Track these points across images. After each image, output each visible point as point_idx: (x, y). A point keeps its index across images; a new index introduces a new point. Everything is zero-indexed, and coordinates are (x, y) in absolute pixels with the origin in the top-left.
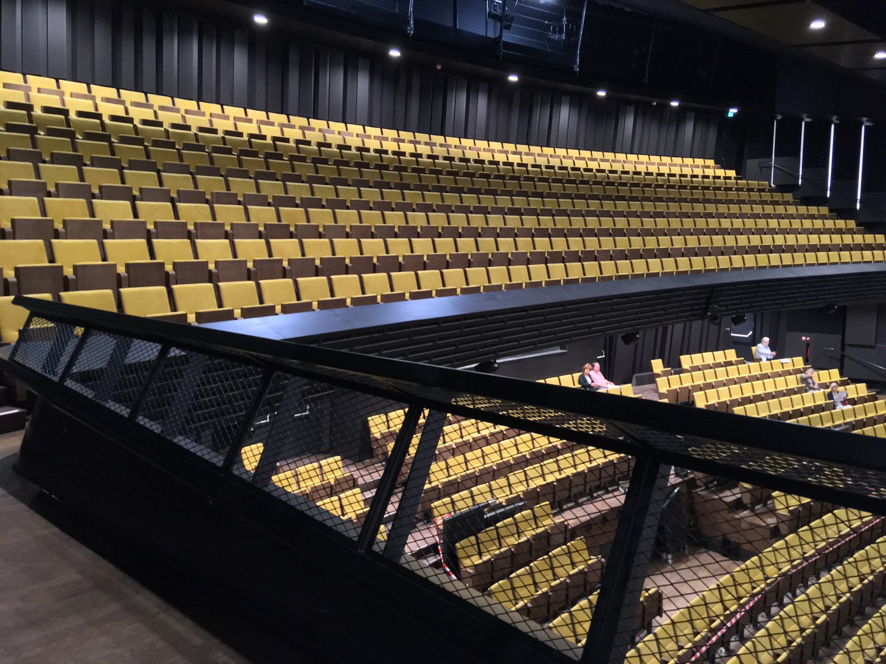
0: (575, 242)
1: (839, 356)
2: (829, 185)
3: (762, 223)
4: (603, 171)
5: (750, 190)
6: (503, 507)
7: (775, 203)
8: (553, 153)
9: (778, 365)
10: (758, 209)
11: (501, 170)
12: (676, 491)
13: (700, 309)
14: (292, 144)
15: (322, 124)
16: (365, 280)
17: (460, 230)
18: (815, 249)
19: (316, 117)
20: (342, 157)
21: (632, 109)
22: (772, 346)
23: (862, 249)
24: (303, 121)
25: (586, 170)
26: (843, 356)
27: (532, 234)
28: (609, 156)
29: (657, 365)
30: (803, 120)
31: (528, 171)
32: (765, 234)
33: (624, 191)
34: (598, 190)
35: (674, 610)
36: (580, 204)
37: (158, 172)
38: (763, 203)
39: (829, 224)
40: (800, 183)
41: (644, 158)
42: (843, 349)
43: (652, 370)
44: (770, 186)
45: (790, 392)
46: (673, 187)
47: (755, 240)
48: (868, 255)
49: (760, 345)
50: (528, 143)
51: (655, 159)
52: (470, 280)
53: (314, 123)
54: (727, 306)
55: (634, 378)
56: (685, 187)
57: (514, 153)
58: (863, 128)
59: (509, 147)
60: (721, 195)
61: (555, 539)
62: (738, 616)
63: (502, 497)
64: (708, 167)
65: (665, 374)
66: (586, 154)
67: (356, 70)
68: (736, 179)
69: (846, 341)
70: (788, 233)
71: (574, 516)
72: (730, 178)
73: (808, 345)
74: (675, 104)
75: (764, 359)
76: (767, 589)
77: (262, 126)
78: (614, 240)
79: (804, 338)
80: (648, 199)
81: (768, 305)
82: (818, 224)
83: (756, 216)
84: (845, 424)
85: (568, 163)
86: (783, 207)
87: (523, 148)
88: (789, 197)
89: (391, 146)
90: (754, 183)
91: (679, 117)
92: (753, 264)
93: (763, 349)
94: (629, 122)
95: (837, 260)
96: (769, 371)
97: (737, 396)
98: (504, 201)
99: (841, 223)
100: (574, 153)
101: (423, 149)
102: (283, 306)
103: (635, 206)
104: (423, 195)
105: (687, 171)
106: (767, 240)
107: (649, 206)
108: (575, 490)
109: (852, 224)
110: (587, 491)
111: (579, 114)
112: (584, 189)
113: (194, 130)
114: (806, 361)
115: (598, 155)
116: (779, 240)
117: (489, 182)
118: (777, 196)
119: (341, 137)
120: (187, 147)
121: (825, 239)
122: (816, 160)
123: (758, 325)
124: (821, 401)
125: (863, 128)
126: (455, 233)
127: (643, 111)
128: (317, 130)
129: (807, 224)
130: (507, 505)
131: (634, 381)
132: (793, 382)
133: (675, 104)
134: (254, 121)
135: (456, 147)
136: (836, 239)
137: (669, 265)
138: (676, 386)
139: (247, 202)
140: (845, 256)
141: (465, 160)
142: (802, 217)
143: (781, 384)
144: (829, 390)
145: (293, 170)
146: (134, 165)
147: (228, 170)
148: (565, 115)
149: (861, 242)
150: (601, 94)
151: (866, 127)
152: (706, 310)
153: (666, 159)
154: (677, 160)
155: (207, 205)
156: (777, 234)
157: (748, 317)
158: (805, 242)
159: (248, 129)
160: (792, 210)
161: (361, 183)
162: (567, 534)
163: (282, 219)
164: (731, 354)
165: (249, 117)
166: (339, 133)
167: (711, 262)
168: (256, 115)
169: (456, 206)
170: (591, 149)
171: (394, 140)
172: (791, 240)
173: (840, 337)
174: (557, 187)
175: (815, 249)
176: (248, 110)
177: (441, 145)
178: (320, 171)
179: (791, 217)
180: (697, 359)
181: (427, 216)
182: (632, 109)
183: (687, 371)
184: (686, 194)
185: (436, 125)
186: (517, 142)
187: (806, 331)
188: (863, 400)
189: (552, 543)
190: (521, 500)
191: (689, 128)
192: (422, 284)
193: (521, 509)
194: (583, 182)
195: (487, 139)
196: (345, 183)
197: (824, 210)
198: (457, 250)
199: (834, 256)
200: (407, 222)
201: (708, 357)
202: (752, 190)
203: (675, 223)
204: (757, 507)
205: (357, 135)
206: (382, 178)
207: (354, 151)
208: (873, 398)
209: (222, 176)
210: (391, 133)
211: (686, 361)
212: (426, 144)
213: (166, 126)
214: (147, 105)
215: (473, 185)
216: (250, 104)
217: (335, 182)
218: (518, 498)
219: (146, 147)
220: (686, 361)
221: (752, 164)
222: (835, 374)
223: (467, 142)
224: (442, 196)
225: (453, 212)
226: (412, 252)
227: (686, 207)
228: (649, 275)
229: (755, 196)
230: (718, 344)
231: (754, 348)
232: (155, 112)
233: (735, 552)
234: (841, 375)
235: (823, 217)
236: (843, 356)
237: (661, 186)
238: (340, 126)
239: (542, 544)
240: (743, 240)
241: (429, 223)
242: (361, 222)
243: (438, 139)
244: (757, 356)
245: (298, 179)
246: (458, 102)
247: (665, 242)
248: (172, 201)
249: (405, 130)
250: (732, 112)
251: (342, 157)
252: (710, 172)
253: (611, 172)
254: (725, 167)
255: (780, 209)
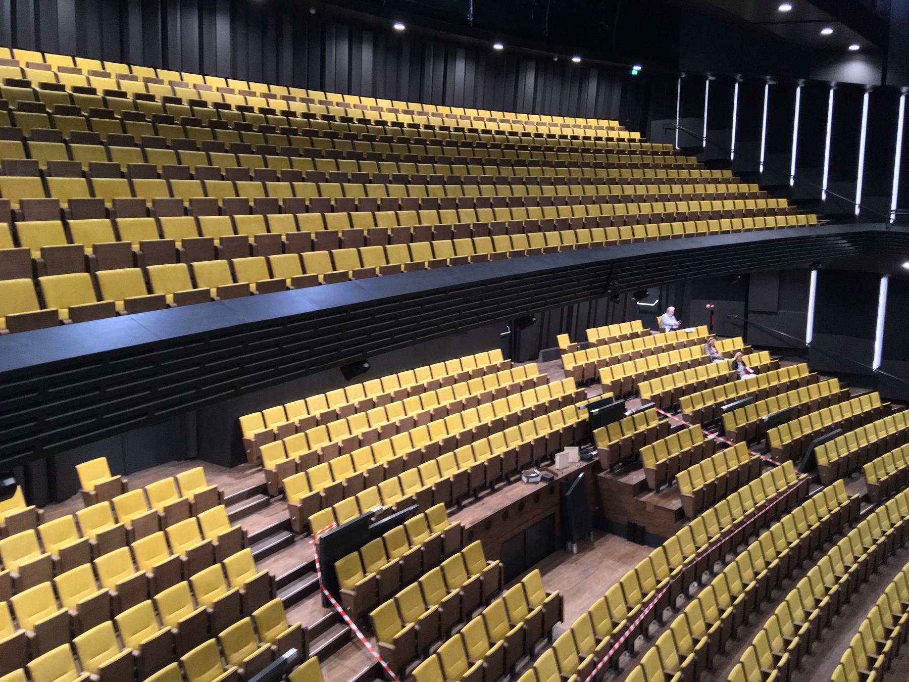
0: (467, 214)
1: (742, 323)
2: (733, 147)
3: (665, 189)
4: (503, 133)
5: (655, 153)
6: (394, 512)
7: (679, 167)
8: (449, 113)
9: (683, 335)
10: (662, 174)
11: (388, 132)
12: (581, 476)
13: (600, 286)
14: (211, 108)
15: (173, 76)
16: (196, 270)
17: (333, 203)
18: (718, 215)
19: (165, 68)
20: (193, 115)
21: (532, 65)
22: (677, 315)
23: (765, 215)
24: (149, 72)
25: (485, 132)
26: (746, 323)
27: (417, 206)
28: (510, 116)
29: (564, 341)
30: (707, 78)
31: (419, 134)
32: (669, 201)
33: (524, 155)
34: (496, 154)
35: (574, 616)
36: (506, 172)
37: (24, 140)
38: (667, 167)
39: (733, 188)
40: (704, 145)
41: (546, 119)
42: (746, 316)
43: (558, 345)
44: (675, 149)
45: (695, 363)
46: (576, 150)
47: (659, 208)
48: (770, 220)
49: (665, 315)
50: (421, 101)
51: (558, 120)
52: (337, 264)
53: (164, 74)
54: (627, 281)
55: (540, 354)
56: (588, 151)
57: (405, 112)
58: (767, 87)
59: (400, 105)
60: (625, 159)
61: (449, 546)
62: (642, 616)
63: (391, 501)
64: (612, 129)
65: (572, 349)
66: (485, 114)
67: (213, 13)
68: (640, 141)
69: (749, 309)
70: (692, 200)
71: (469, 517)
72: (633, 140)
73: (712, 312)
74: (576, 60)
75: (667, 329)
76: (672, 581)
77: (121, 81)
78: (511, 211)
79: (708, 306)
80: (549, 164)
81: (670, 278)
82: (722, 189)
83: (660, 182)
84: (749, 394)
85: (464, 124)
86: (697, 171)
87: (415, 107)
88: (693, 160)
89: (278, 105)
90: (658, 146)
91: (582, 74)
92: (656, 235)
93: (668, 319)
94: (530, 79)
95: (740, 227)
96: (674, 342)
97: (643, 370)
98: (389, 168)
99: (744, 188)
100: (471, 113)
101: (298, 107)
102: (71, 311)
103: (535, 172)
104: (314, 162)
105: (591, 133)
106: (671, 207)
107: (550, 172)
108: (474, 485)
109: (755, 188)
110: (488, 484)
111: (476, 72)
112: (480, 153)
113: (69, 90)
114: (711, 330)
115: (497, 115)
116: (683, 207)
117: (372, 145)
118: (682, 160)
119: (219, 94)
120: (61, 110)
121: (729, 205)
122: (720, 122)
123: (664, 295)
124: (725, 372)
125: (767, 87)
126: (324, 206)
127: (545, 68)
128: (214, 89)
129: (711, 189)
130: (398, 511)
131: (541, 358)
132: (696, 352)
133: (576, 60)
134: (113, 76)
135: (338, 104)
136: (740, 204)
137: (569, 238)
138: (582, 362)
139: (170, 173)
140: (749, 222)
141: (347, 120)
142: (706, 181)
143: (686, 355)
144: (734, 359)
145: (125, 131)
146: (40, 136)
147: (110, 137)
148: (460, 70)
149: (764, 207)
150: (498, 47)
151: (770, 86)
152: (606, 287)
153: (570, 121)
154: (581, 121)
155: (83, 179)
156: (680, 200)
157: (650, 291)
158: (708, 209)
159: (101, 85)
160: (695, 174)
161: (266, 150)
162: (464, 536)
163: (97, 192)
164: (637, 326)
165: (107, 70)
166: (195, 86)
167: (613, 234)
168: (87, 64)
169: (331, 174)
170: (490, 109)
171: (264, 96)
172: (694, 206)
173: (743, 303)
174: (450, 151)
175: (718, 215)
176: (77, 58)
177: (321, 102)
178: (160, 132)
179: (694, 181)
180: (604, 332)
181: (292, 186)
182: (532, 65)
183: (593, 345)
184: (589, 158)
185: (318, 81)
186: (408, 100)
187: (710, 299)
188: (766, 368)
189: (447, 551)
190: (414, 502)
191: (592, 87)
192: (276, 271)
193: (414, 513)
194: (481, 145)
195: (375, 96)
196: (248, 150)
197: (728, 174)
198: (326, 228)
199: (737, 223)
200: (267, 194)
201: (615, 330)
202: (656, 153)
203: (577, 191)
204: (661, 488)
205: (218, 89)
206: (267, 142)
207: (234, 111)
208: (776, 366)
209: (102, 143)
210: (259, 88)
211: (593, 334)
212: (302, 100)
213: (69, 90)
214: (13, 62)
215: (354, 148)
216: (81, 51)
217: (237, 149)
218: (409, 501)
219: (10, 111)
220: (593, 334)
221: (656, 125)
222: (738, 343)
223: (352, 100)
224: (314, 162)
225: (349, 181)
226: (269, 231)
227: (589, 173)
228: (530, 252)
229: (659, 159)
230: (624, 315)
231: (659, 318)
232: (22, 70)
233: (642, 536)
234: (745, 341)
235: (727, 182)
236: (746, 323)
237: (563, 150)
238: (197, 79)
239: (437, 552)
240: (646, 208)
241: (294, 195)
242: (206, 195)
243: (317, 95)
244: (661, 327)
245: (192, 146)
246: (339, 54)
247: (565, 212)
248: (42, 174)
249: (277, 84)
250: (636, 70)
251: (193, 115)
252: (614, 134)
253: (512, 134)
254: (630, 129)
255: (684, 174)
